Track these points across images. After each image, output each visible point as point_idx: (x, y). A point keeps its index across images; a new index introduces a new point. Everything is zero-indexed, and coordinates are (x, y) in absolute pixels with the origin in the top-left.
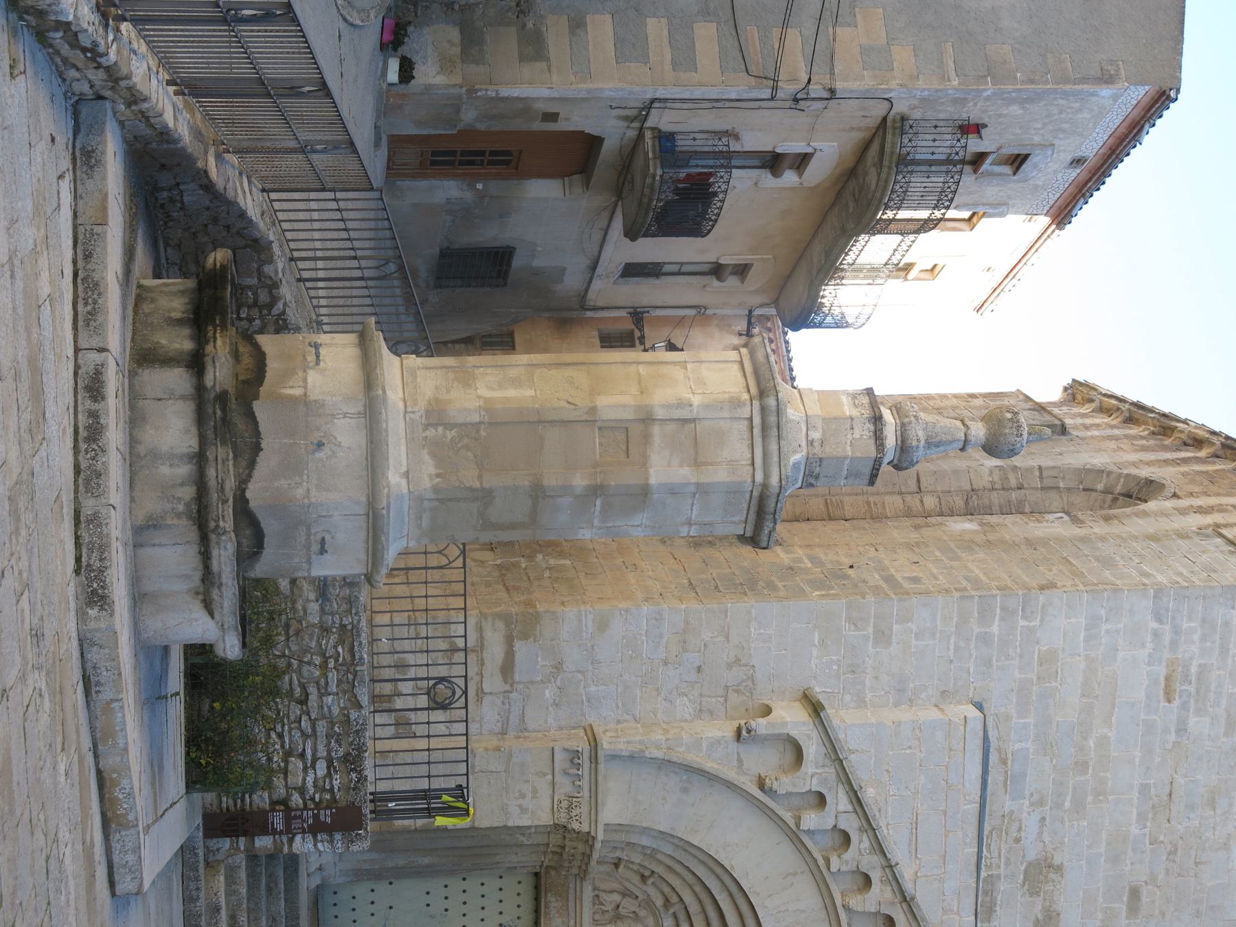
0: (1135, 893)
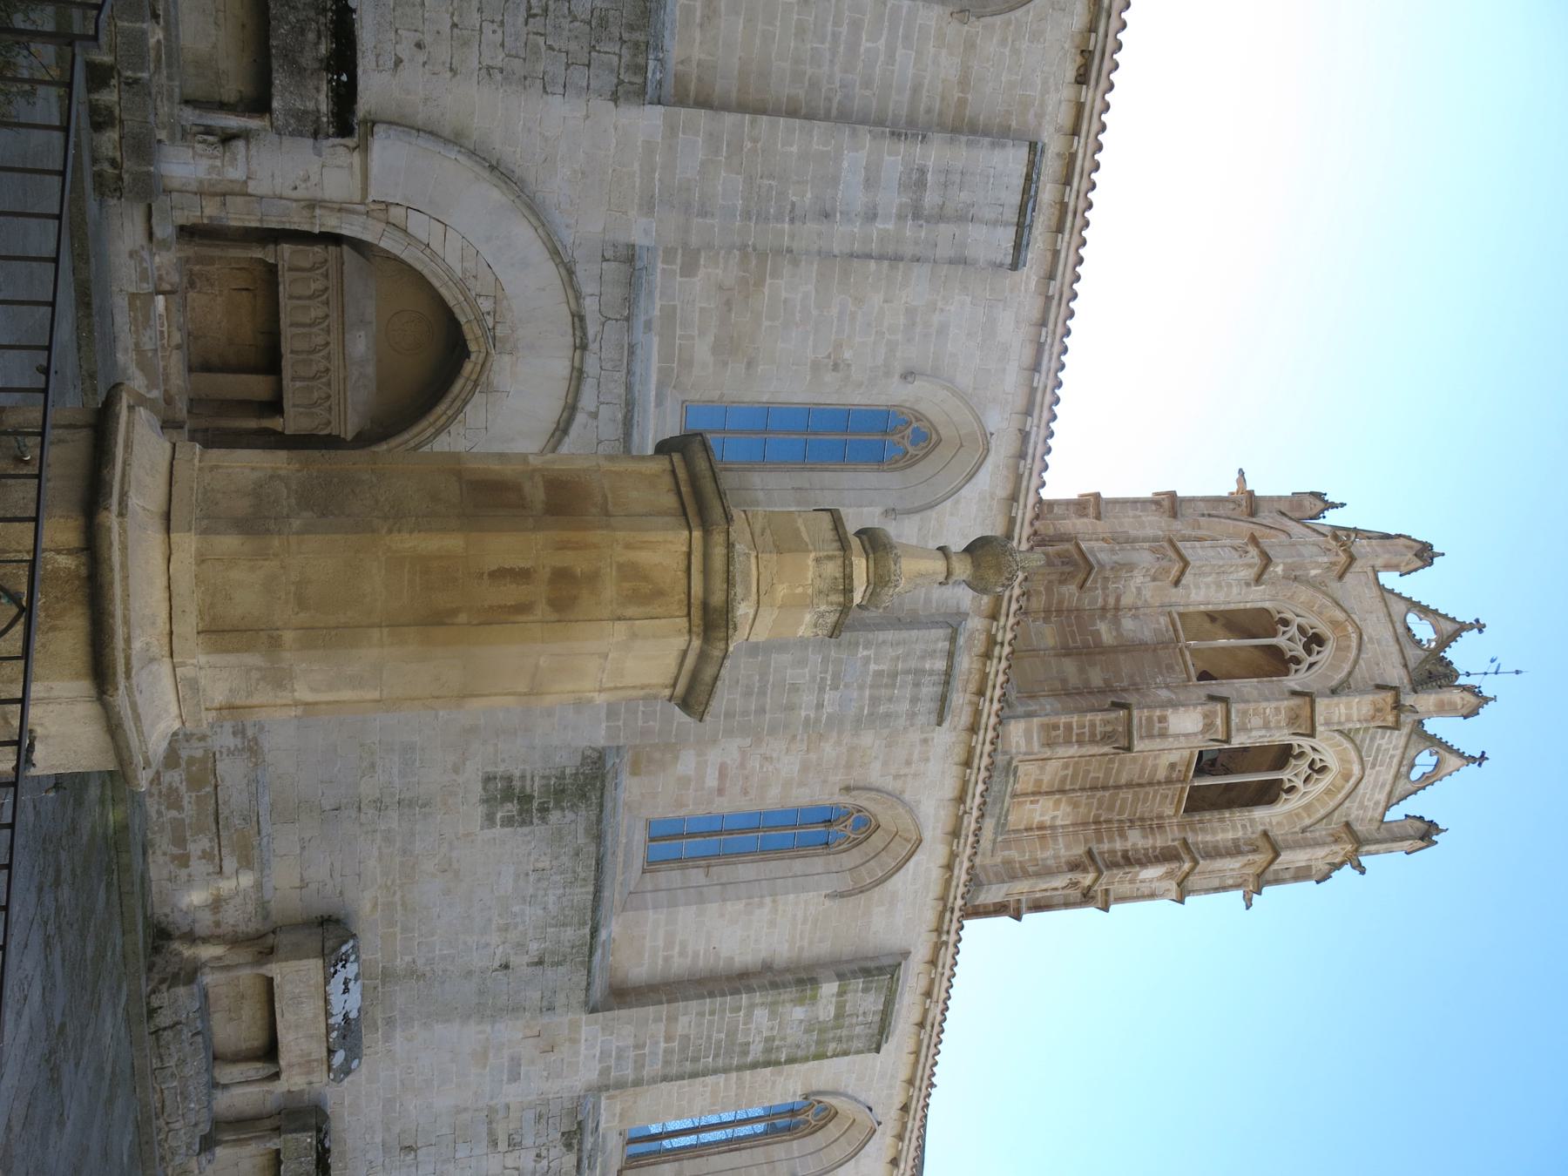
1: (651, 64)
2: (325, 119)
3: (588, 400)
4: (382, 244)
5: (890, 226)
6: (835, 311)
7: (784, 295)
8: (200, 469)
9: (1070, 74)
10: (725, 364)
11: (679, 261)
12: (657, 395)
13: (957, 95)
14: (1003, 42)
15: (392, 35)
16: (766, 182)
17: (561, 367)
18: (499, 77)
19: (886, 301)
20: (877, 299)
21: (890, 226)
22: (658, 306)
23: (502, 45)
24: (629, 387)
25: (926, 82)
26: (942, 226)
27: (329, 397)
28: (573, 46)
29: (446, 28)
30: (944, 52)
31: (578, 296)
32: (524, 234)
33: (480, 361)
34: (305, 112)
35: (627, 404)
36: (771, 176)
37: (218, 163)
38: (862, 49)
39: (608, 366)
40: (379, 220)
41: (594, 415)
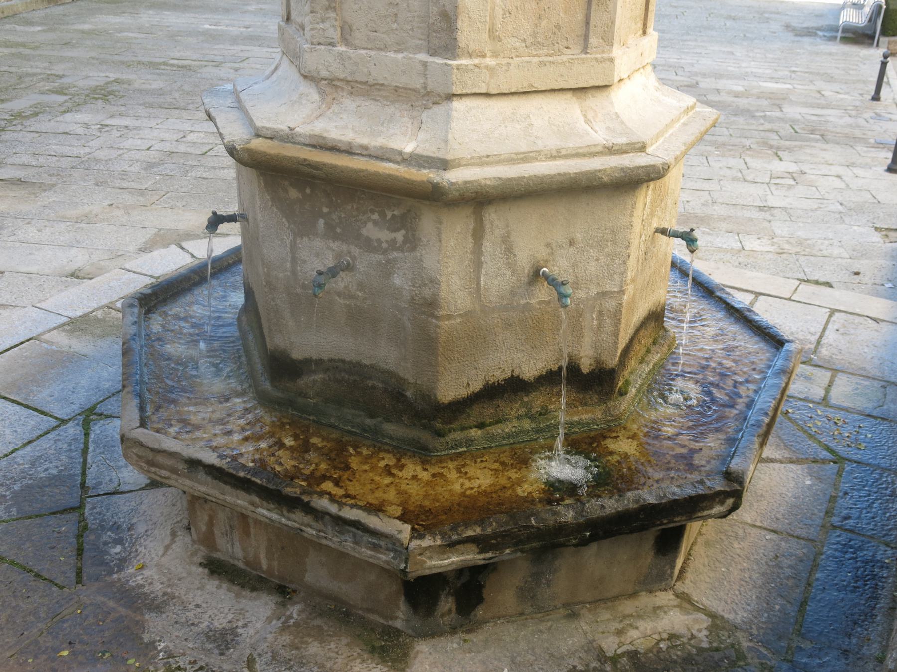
8: (495, 55)
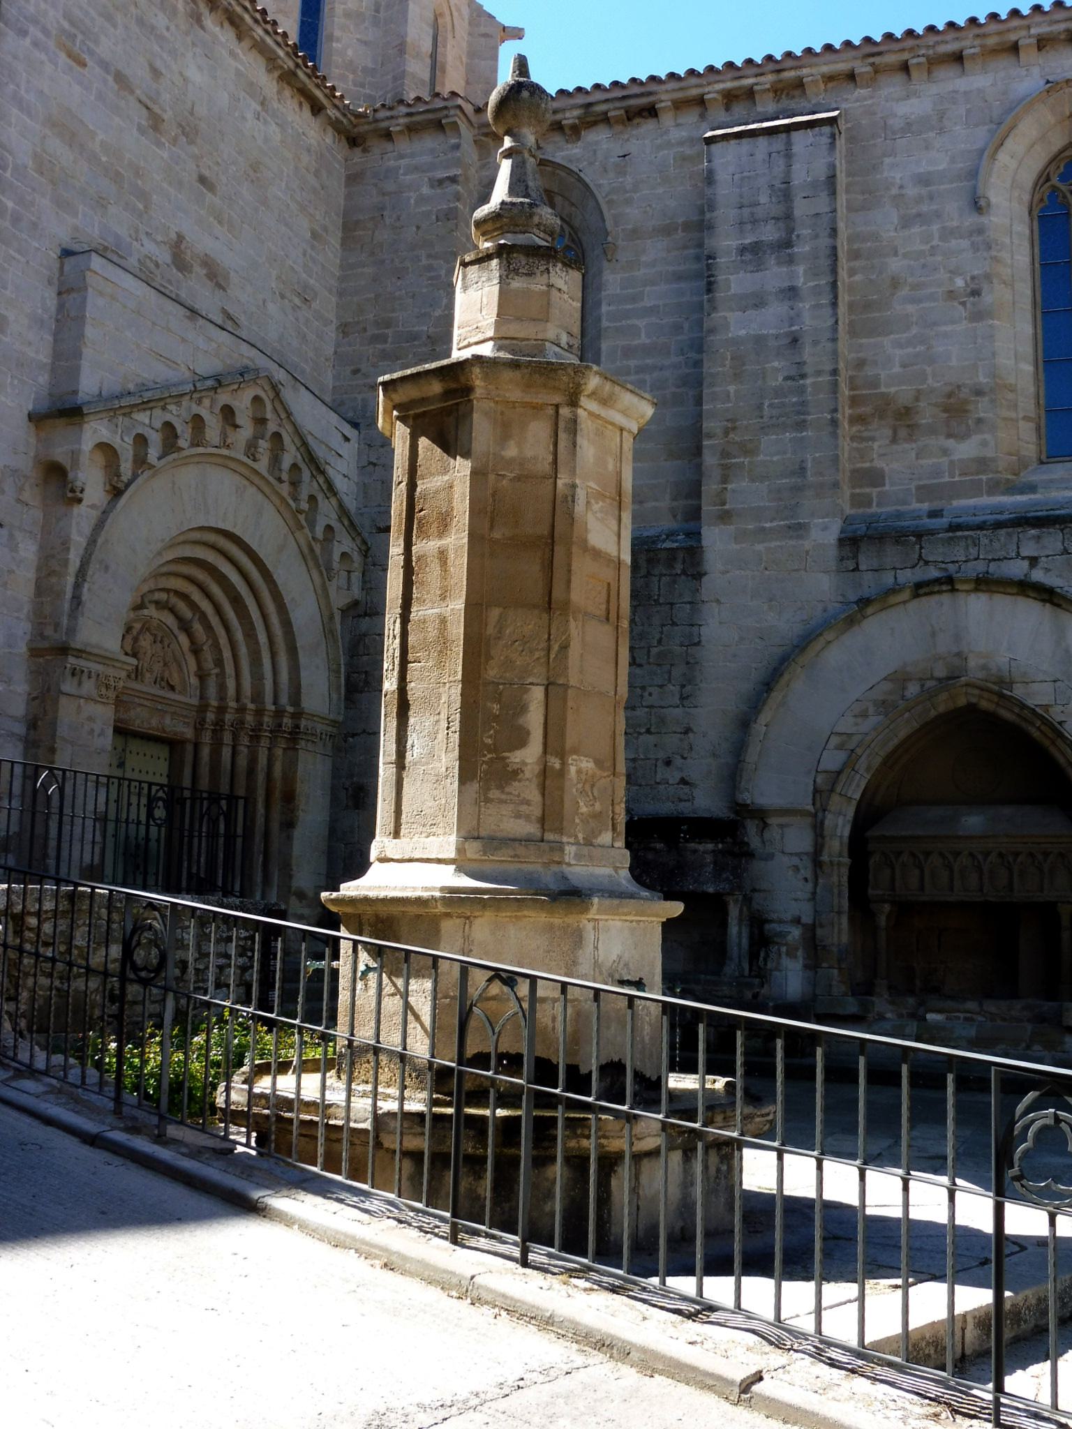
0: (202, 180)
1: (668, 545)
2: (720, 846)
3: (1017, 569)
4: (857, 796)
5: (801, 269)
6: (911, 308)
7: (897, 369)
9: (649, 126)
10: (980, 421)
11: (867, 490)
12: (1022, 493)
13: (680, 234)
14: (628, 202)
15: (661, 787)
16: (766, 411)
17: (976, 606)
18: (688, 688)
19: (896, 254)
20: (895, 265)
21: (801, 269)
22: (918, 506)
23: (661, 686)
24: (998, 525)
25: (671, 268)
26: (797, 213)
27: (1031, 855)
28: (656, 620)
29: (651, 739)
30: (643, 259)
31: (893, 591)
32: (837, 654)
33: (976, 692)
34: (715, 863)
35: (1019, 525)
36: (760, 407)
37: (784, 949)
38: (648, 341)
39: (973, 552)
40: (829, 797)
41: (1034, 561)
